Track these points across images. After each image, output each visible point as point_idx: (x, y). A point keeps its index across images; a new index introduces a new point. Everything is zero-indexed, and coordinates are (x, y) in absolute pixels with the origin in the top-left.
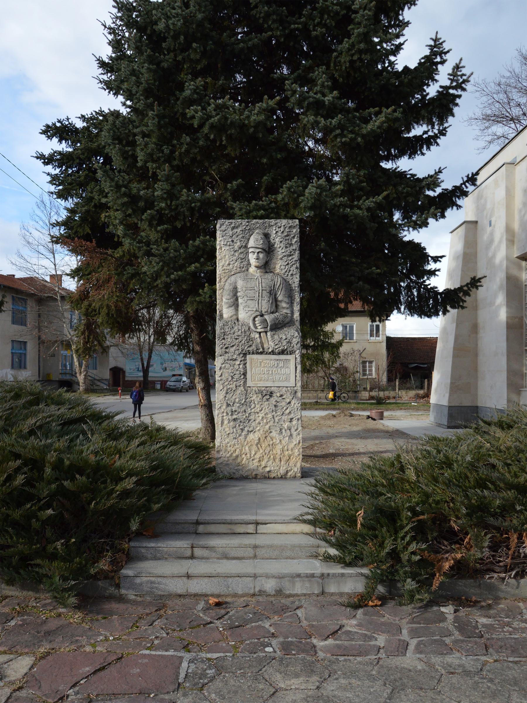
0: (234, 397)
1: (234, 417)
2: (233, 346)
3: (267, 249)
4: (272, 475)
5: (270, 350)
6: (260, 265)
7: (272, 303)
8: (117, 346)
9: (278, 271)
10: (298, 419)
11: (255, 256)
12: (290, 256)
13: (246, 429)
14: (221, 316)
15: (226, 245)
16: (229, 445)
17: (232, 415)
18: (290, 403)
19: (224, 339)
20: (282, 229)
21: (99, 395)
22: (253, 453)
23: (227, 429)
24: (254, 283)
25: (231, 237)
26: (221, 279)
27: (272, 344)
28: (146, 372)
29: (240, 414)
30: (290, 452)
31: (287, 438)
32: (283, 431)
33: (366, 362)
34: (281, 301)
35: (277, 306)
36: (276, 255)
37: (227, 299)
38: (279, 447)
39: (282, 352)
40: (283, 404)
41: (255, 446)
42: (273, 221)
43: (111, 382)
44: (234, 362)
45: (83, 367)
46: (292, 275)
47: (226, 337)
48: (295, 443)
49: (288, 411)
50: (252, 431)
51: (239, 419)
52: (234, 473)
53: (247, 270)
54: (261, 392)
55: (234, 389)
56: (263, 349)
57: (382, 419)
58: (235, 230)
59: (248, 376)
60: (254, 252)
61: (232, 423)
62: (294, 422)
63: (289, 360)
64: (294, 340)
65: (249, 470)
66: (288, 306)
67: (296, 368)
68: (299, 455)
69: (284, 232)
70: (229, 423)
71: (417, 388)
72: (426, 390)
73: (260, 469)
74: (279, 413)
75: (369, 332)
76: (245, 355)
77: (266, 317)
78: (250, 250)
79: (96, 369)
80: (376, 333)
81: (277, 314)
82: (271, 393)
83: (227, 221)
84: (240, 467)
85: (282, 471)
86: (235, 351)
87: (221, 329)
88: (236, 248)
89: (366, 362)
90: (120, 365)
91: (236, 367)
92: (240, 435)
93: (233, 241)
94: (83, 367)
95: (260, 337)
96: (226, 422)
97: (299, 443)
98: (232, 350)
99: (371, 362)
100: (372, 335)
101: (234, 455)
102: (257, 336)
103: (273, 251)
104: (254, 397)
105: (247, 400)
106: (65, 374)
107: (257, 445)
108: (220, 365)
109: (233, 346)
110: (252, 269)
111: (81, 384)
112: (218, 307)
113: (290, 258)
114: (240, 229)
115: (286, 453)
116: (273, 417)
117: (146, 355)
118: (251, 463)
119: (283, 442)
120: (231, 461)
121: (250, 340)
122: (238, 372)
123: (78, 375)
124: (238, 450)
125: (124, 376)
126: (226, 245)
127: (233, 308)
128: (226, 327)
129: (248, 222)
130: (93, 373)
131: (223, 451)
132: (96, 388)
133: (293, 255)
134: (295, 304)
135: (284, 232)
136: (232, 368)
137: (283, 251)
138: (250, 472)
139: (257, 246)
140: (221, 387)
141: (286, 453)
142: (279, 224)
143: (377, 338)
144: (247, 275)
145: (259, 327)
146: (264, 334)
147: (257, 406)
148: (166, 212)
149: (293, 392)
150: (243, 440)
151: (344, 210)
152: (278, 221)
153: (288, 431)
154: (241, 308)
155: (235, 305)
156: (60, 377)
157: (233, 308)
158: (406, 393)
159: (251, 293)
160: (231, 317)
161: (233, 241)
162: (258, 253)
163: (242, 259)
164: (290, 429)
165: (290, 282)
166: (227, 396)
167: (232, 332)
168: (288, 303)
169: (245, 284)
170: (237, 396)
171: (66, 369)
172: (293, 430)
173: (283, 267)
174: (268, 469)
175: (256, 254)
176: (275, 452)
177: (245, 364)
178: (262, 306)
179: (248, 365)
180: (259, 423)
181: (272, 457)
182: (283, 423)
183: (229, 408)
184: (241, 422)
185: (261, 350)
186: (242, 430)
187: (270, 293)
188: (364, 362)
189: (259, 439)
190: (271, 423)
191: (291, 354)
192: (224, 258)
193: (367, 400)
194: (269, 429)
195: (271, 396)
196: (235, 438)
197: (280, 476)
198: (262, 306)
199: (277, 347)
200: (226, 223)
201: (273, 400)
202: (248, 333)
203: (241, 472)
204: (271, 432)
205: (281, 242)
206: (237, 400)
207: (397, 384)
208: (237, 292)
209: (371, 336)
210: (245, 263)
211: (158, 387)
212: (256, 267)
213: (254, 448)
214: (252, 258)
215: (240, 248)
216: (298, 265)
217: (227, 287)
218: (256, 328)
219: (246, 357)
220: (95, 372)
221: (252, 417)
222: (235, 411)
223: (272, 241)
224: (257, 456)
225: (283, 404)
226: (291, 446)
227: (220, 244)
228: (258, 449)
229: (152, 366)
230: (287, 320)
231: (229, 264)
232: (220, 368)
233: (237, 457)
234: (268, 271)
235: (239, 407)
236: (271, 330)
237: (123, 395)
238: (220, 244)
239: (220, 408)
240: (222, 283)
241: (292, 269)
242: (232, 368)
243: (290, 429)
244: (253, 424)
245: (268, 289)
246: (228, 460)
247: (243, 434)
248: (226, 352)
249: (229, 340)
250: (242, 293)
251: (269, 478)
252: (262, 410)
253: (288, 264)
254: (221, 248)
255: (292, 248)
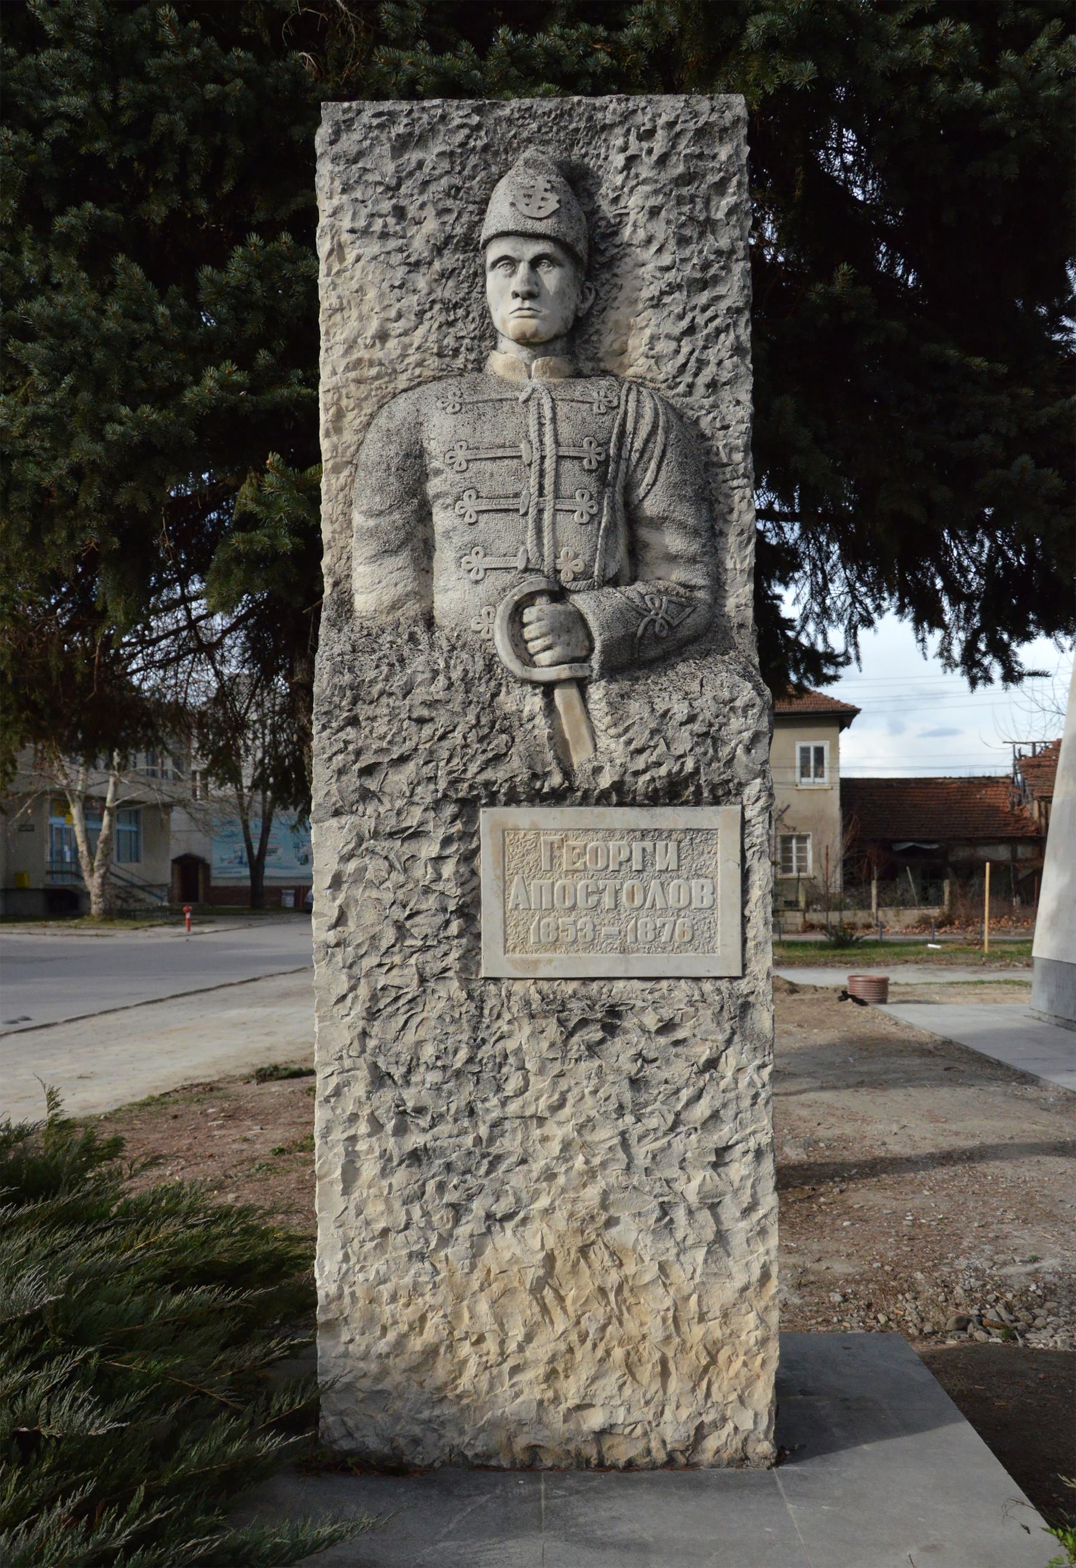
0: (410, 1037)
1: (416, 1140)
2: (403, 759)
3: (581, 247)
4: (622, 1452)
5: (605, 781)
6: (548, 330)
7: (611, 530)
8: (183, 803)
9: (638, 365)
10: (759, 1154)
11: (518, 281)
12: (703, 284)
13: (478, 1207)
14: (345, 605)
15: (366, 232)
16: (386, 1290)
17: (401, 1130)
18: (712, 1064)
19: (353, 722)
20: (659, 144)
21: (138, 924)
22: (517, 1333)
23: (375, 1208)
24: (512, 423)
25: (393, 190)
26: (340, 415)
27: (612, 746)
28: (256, 865)
29: (444, 1129)
30: (715, 1329)
31: (700, 1254)
32: (680, 1214)
33: (791, 838)
34: (658, 523)
35: (636, 551)
36: (628, 283)
37: (370, 514)
38: (658, 1301)
39: (673, 792)
40: (679, 1070)
41: (524, 1298)
42: (611, 106)
43: (176, 892)
44: (409, 849)
45: (99, 856)
46: (713, 386)
47: (363, 711)
48: (738, 1284)
49: (702, 1110)
50: (508, 1217)
51: (442, 1152)
52: (416, 1441)
53: (479, 365)
54: (557, 1008)
55: (412, 990)
56: (568, 773)
57: (883, 1001)
58: (413, 156)
59: (489, 920)
60: (510, 262)
61: (400, 1177)
62: (738, 1169)
63: (709, 833)
64: (736, 723)
65: (494, 1425)
66: (694, 547)
67: (745, 875)
68: (763, 1342)
69: (666, 163)
70: (384, 1173)
71: (925, 900)
72: (946, 908)
73: (555, 1417)
74: (653, 1122)
75: (798, 763)
76: (468, 807)
77: (583, 602)
78: (494, 252)
79: (138, 861)
80: (816, 768)
81: (639, 586)
82: (614, 1012)
83: (370, 108)
84: (447, 1410)
85: (673, 1430)
86: (413, 786)
87: (336, 671)
88: (419, 246)
89: (791, 838)
90: (197, 850)
91: (422, 873)
92: (445, 1240)
93: (399, 212)
94: (99, 856)
95: (550, 708)
96: (369, 1169)
97: (765, 1277)
98: (399, 779)
99: (802, 839)
100: (804, 773)
101: (416, 1344)
102: (535, 702)
103: (611, 264)
104: (522, 1036)
105: (485, 1052)
106: (62, 872)
107: (536, 1290)
108: (334, 866)
109: (403, 759)
110: (506, 358)
111: (93, 898)
112: (326, 562)
113: (703, 298)
114: (437, 147)
115: (696, 1333)
116: (625, 1144)
117: (256, 826)
118: (504, 1390)
119: (678, 1275)
120: (397, 1377)
121: (497, 725)
122: (431, 902)
123: (86, 875)
124: (434, 1320)
125: (207, 877)
126: (366, 232)
127: (402, 559)
128: (366, 661)
129: (478, 110)
130: (127, 869)
131: (356, 1324)
132: (133, 905)
133: (716, 280)
134: (732, 540)
135: (666, 163)
136: (397, 877)
137: (666, 259)
138: (501, 1436)
139: (530, 226)
140: (343, 984)
141: (696, 1333)
142: (643, 120)
143: (818, 780)
144: (474, 388)
145: (545, 658)
146: (573, 692)
147: (537, 1083)
148: (99, 146)
149: (731, 1008)
150: (461, 1267)
151: (953, 88)
152: (640, 101)
153: (705, 1216)
154: (445, 556)
155: (416, 542)
156: (48, 880)
157: (402, 559)
158: (897, 915)
159: (498, 477)
160: (394, 607)
161: (399, 212)
162: (535, 263)
163: (450, 307)
164: (713, 1207)
165: (705, 423)
166: (376, 1028)
167: (398, 682)
168: (696, 533)
169: (465, 432)
170: (428, 1030)
171: (62, 860)
172: (730, 1210)
173: (664, 347)
174: (595, 1420)
175: (523, 269)
176: (632, 1327)
177: (469, 857)
178: (556, 545)
179: (485, 863)
180: (550, 1176)
181: (618, 1353)
182: (674, 1172)
183: (387, 1096)
184: (449, 1167)
185: (556, 779)
186: (458, 1210)
187: (601, 473)
188: (786, 840)
189: (550, 1259)
190: (614, 1174)
191: (716, 801)
192: (359, 297)
193: (798, 932)
194: (604, 1206)
195: (610, 1030)
196: (421, 1256)
197: (660, 1456)
198: (556, 545)
199: (640, 763)
200: (365, 118)
201: (621, 1052)
202: (483, 689)
203: (450, 1435)
204: (611, 1222)
205: (654, 212)
206: (428, 1052)
207: (874, 892)
208: (423, 476)
209: (803, 775)
210: (467, 329)
211: (289, 901)
212: (524, 341)
213: (522, 1310)
214: (503, 300)
215: (439, 250)
216: (744, 333)
217: (373, 450)
218: (528, 660)
219: (472, 819)
220: (133, 867)
221: (510, 1144)
222: (420, 1111)
223: (608, 210)
224: (541, 1350)
225: (679, 1070)
226: (723, 1293)
227: (335, 232)
228: (545, 1310)
229: (274, 851)
230: (693, 621)
231: (382, 336)
232: (337, 882)
233: (431, 1353)
234: (587, 367)
235: (437, 1088)
236: (610, 671)
237: (201, 923)
238: (335, 232)
239: (337, 1092)
240: (349, 437)
241: (711, 355)
242: (397, 877)
243: (713, 1207)
244: (517, 1180)
245: (591, 455)
246: (384, 1373)
247: (463, 1230)
248: (366, 795)
249: (381, 727)
250: (450, 475)
251: (601, 1466)
252: (561, 1104)
253: (691, 330)
254: (338, 250)
255: (711, 243)
